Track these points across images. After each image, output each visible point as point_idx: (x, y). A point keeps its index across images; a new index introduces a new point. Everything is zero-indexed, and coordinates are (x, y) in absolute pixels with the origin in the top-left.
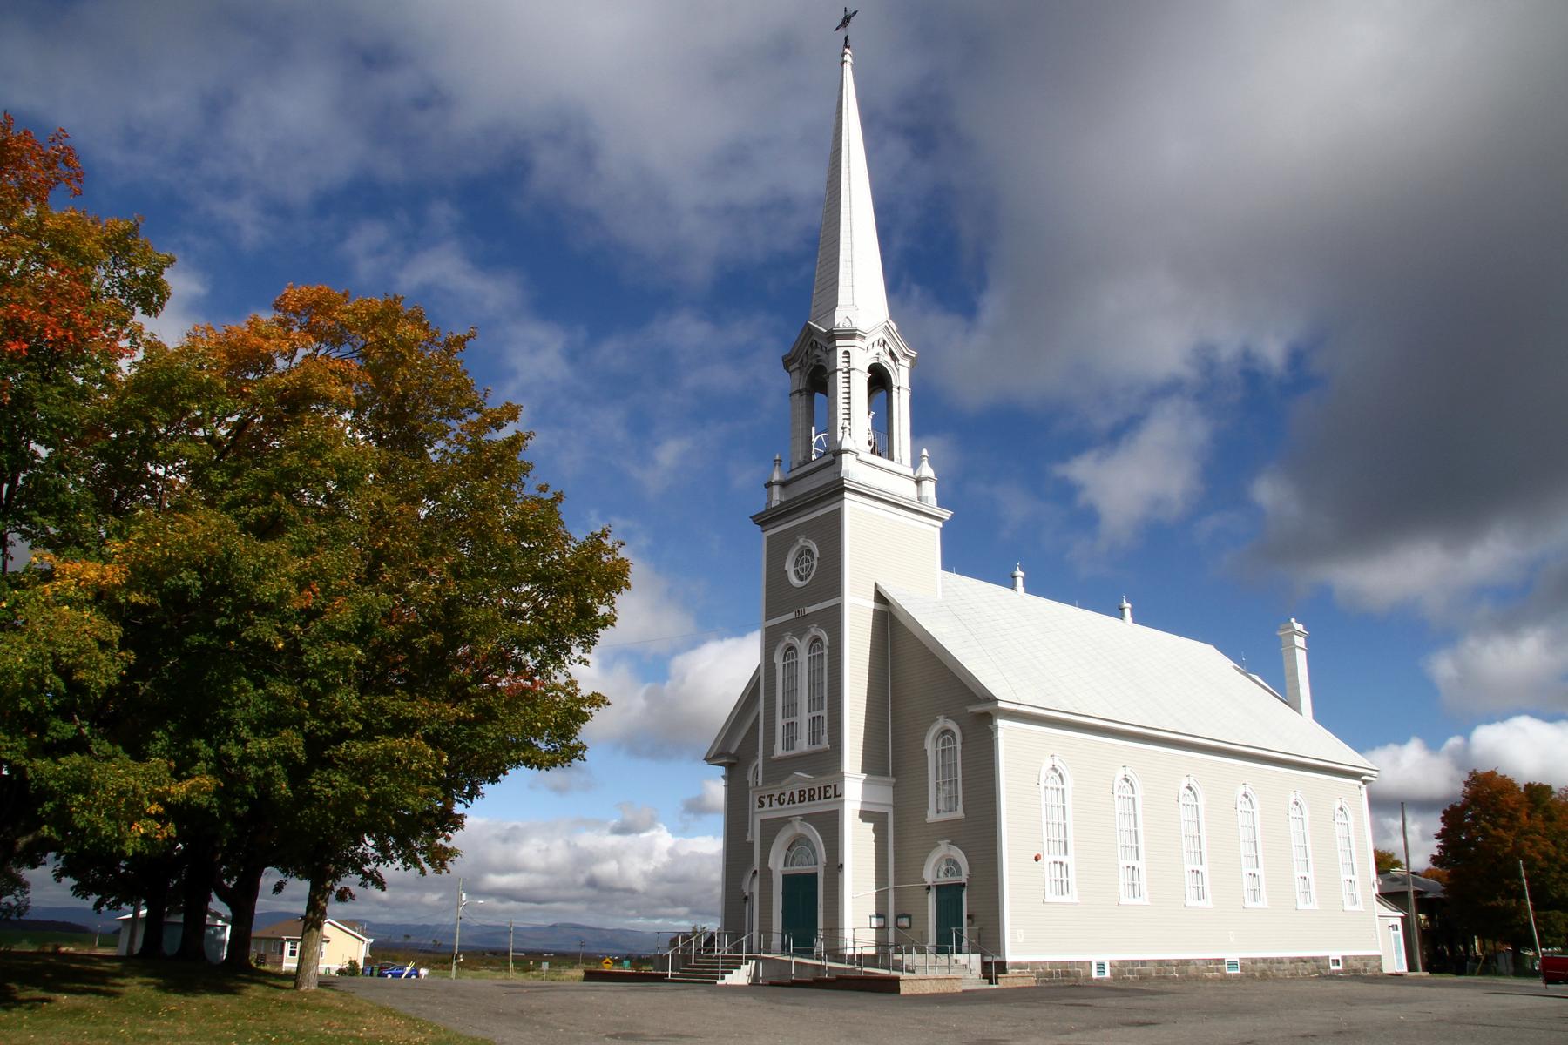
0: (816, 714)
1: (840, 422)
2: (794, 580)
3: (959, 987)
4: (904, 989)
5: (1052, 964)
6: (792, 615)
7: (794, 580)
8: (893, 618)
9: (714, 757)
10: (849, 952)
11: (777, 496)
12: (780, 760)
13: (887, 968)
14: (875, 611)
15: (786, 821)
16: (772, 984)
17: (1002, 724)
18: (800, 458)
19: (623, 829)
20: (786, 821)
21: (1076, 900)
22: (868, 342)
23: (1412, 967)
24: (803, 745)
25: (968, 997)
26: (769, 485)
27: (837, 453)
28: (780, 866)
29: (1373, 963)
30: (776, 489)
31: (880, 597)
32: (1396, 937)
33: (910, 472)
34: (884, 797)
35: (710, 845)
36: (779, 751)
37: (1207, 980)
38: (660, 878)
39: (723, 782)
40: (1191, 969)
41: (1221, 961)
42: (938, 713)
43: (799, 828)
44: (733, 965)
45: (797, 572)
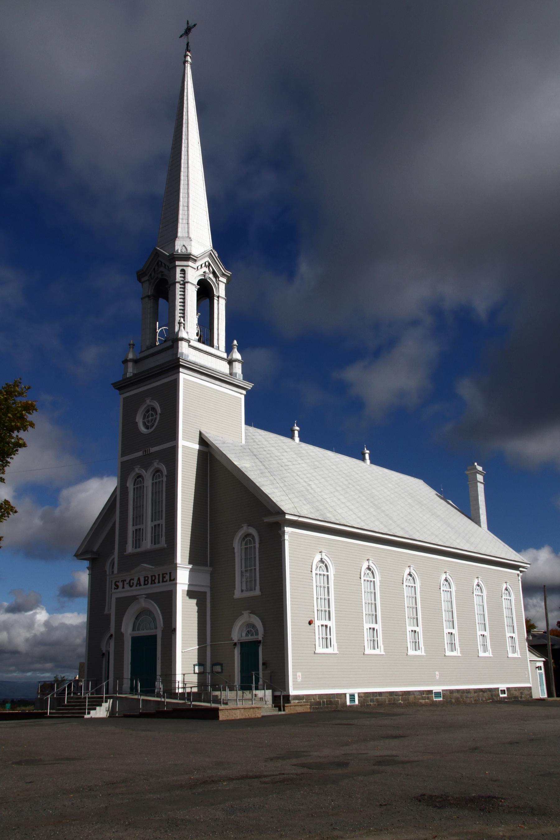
0: (157, 523)
1: (177, 319)
2: (143, 429)
3: (259, 714)
5: (321, 696)
6: (140, 454)
7: (143, 429)
8: (211, 455)
9: (80, 555)
10: (181, 691)
11: (131, 370)
12: (131, 555)
13: (209, 702)
14: (199, 451)
15: (134, 598)
16: (126, 716)
17: (288, 530)
18: (148, 343)
19: (15, 609)
20: (134, 598)
21: (336, 651)
22: (198, 263)
23: (550, 694)
24: (147, 544)
25: (265, 721)
26: (125, 362)
27: (174, 340)
29: (526, 692)
30: (130, 365)
31: (203, 441)
32: (540, 675)
33: (225, 355)
34: (205, 580)
35: (76, 619)
36: (130, 549)
37: (422, 705)
38: (37, 642)
39: (88, 572)
40: (411, 698)
41: (430, 692)
42: (245, 526)
43: (144, 603)
44: (96, 703)
45: (144, 424)
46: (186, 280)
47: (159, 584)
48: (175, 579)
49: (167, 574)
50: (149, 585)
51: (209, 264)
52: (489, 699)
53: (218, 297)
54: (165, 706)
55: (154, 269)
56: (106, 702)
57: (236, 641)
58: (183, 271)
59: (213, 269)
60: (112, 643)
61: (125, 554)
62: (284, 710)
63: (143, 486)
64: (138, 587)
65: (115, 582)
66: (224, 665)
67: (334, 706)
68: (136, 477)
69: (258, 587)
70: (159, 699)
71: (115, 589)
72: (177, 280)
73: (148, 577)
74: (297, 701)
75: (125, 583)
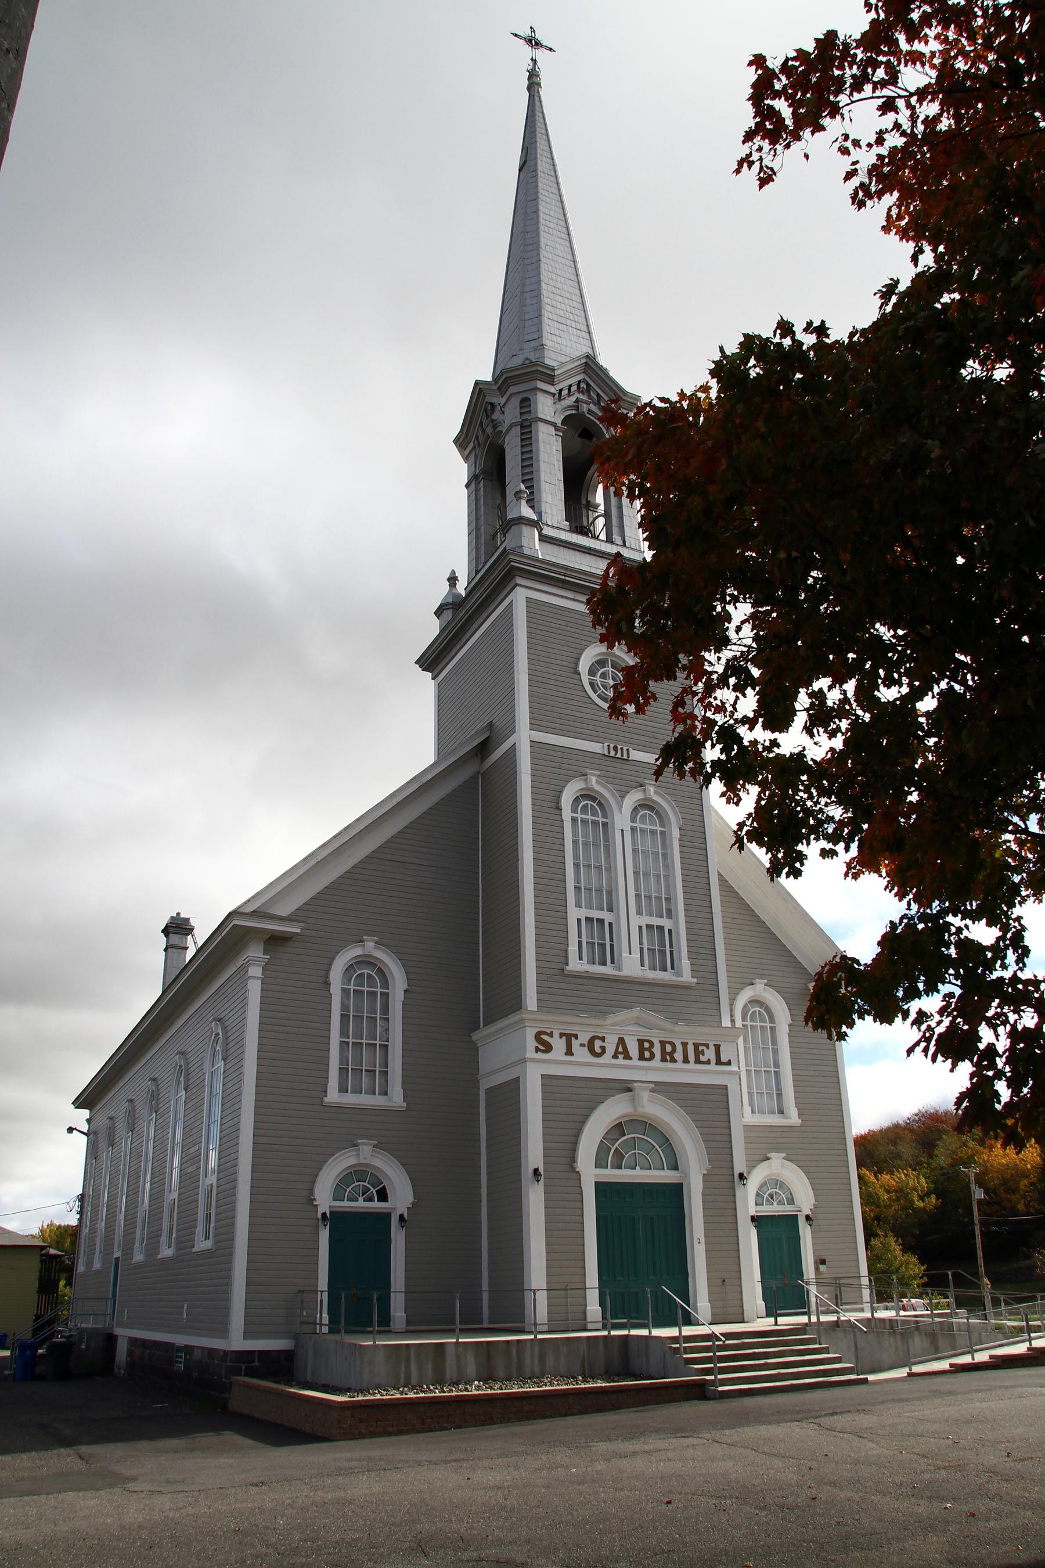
15: (626, 1087)
47: (686, 1066)
50: (656, 1062)
51: (588, 385)
73: (652, 1044)
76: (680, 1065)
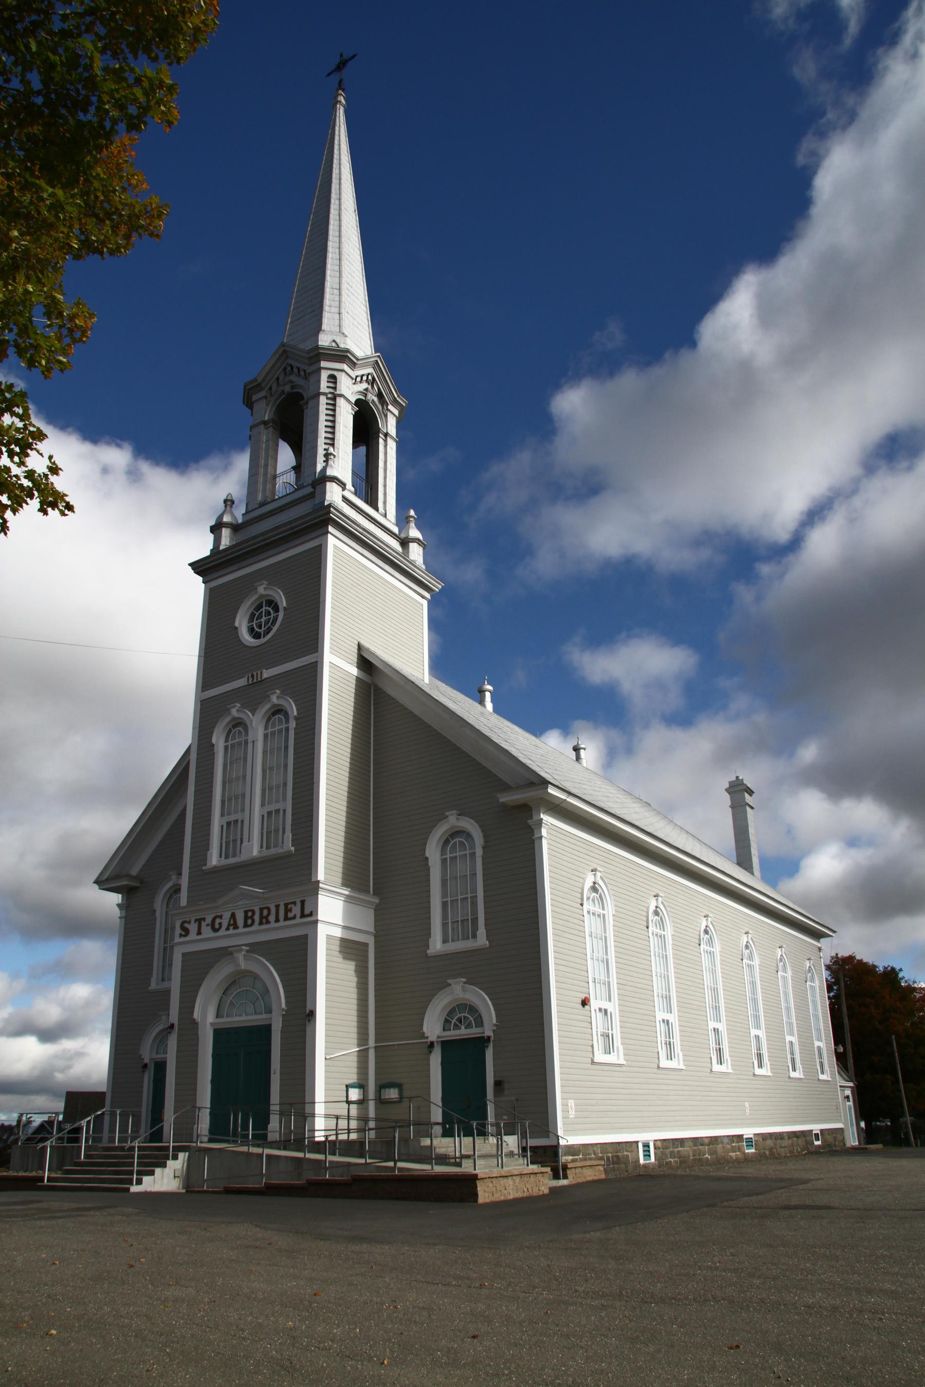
4: (484, 1194)
6: (242, 682)
8: (379, 692)
12: (217, 870)
14: (358, 679)
15: (225, 953)
16: (228, 1191)
24: (253, 849)
28: (211, 1018)
31: (366, 663)
34: (366, 921)
36: (214, 859)
41: (740, 1137)
44: (155, 1159)
45: (251, 630)
46: (338, 392)
47: (277, 925)
48: (313, 913)
49: (294, 903)
50: (256, 927)
51: (373, 378)
52: (803, 1150)
53: (386, 435)
54: (326, 1168)
55: (278, 379)
56: (175, 1157)
57: (433, 1038)
58: (333, 379)
59: (379, 389)
60: (173, 1042)
61: (204, 868)
62: (565, 1177)
63: (246, 742)
64: (231, 931)
65: (183, 923)
66: (405, 1087)
67: (623, 1166)
68: (230, 726)
69: (482, 931)
70: (301, 1155)
71: (181, 935)
72: (322, 390)
74: (570, 1158)
75: (204, 924)
76: (273, 925)
